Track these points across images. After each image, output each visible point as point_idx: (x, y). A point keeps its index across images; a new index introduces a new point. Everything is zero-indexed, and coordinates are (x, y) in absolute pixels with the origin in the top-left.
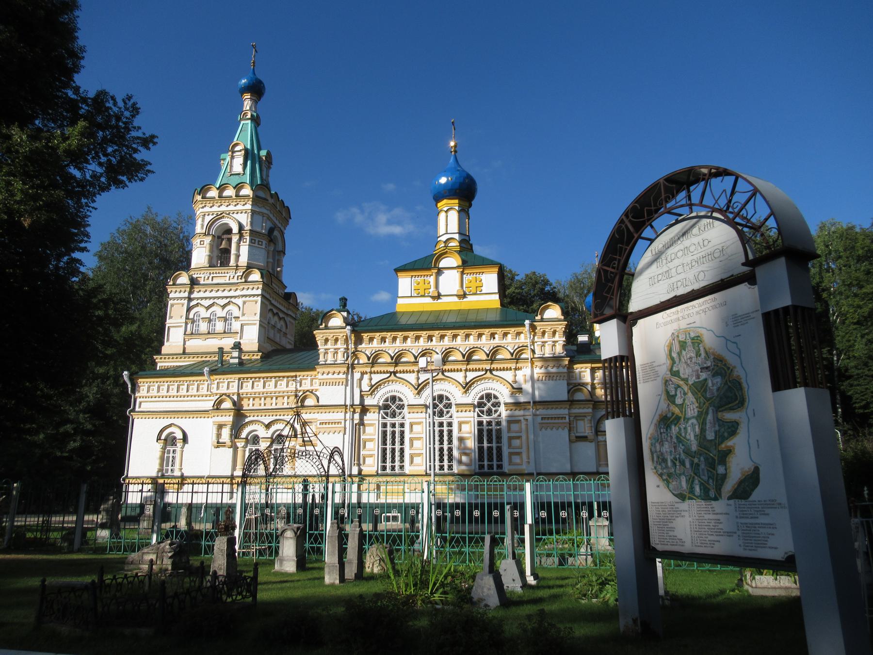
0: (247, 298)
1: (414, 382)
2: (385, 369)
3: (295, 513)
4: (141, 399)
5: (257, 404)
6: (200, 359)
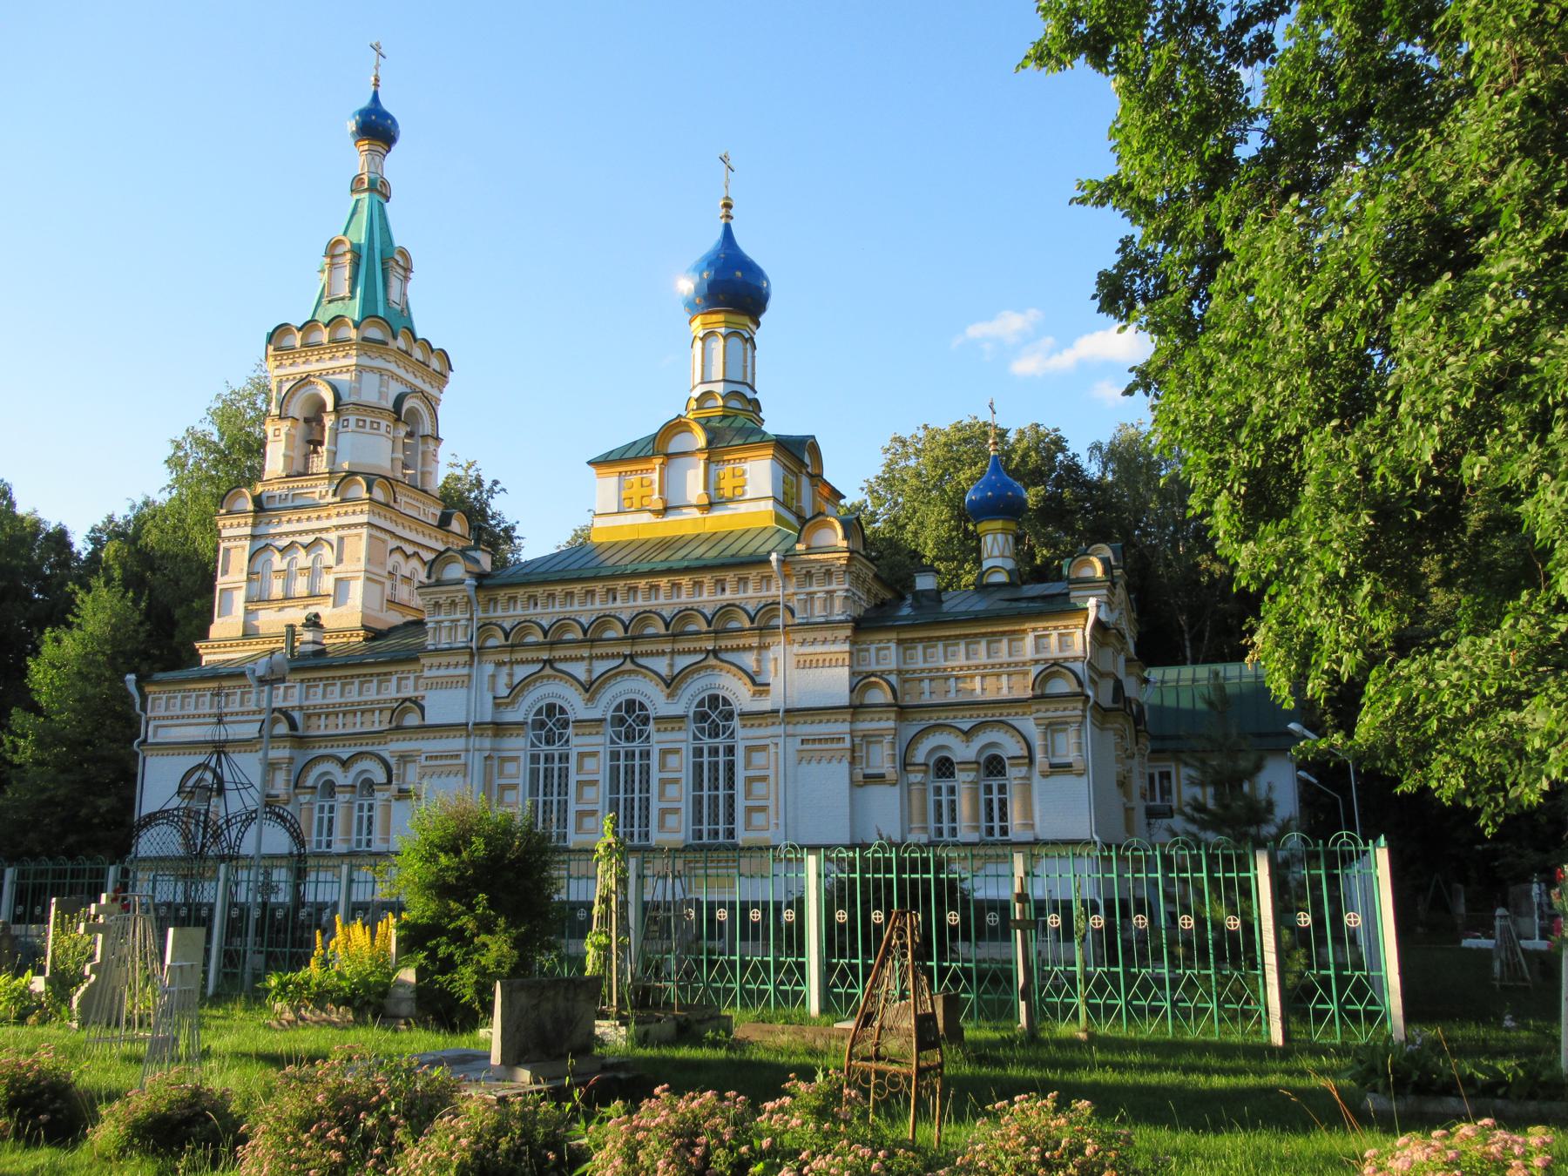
1: (583, 677)
2: (615, 650)
3: (711, 919)
4: (158, 723)
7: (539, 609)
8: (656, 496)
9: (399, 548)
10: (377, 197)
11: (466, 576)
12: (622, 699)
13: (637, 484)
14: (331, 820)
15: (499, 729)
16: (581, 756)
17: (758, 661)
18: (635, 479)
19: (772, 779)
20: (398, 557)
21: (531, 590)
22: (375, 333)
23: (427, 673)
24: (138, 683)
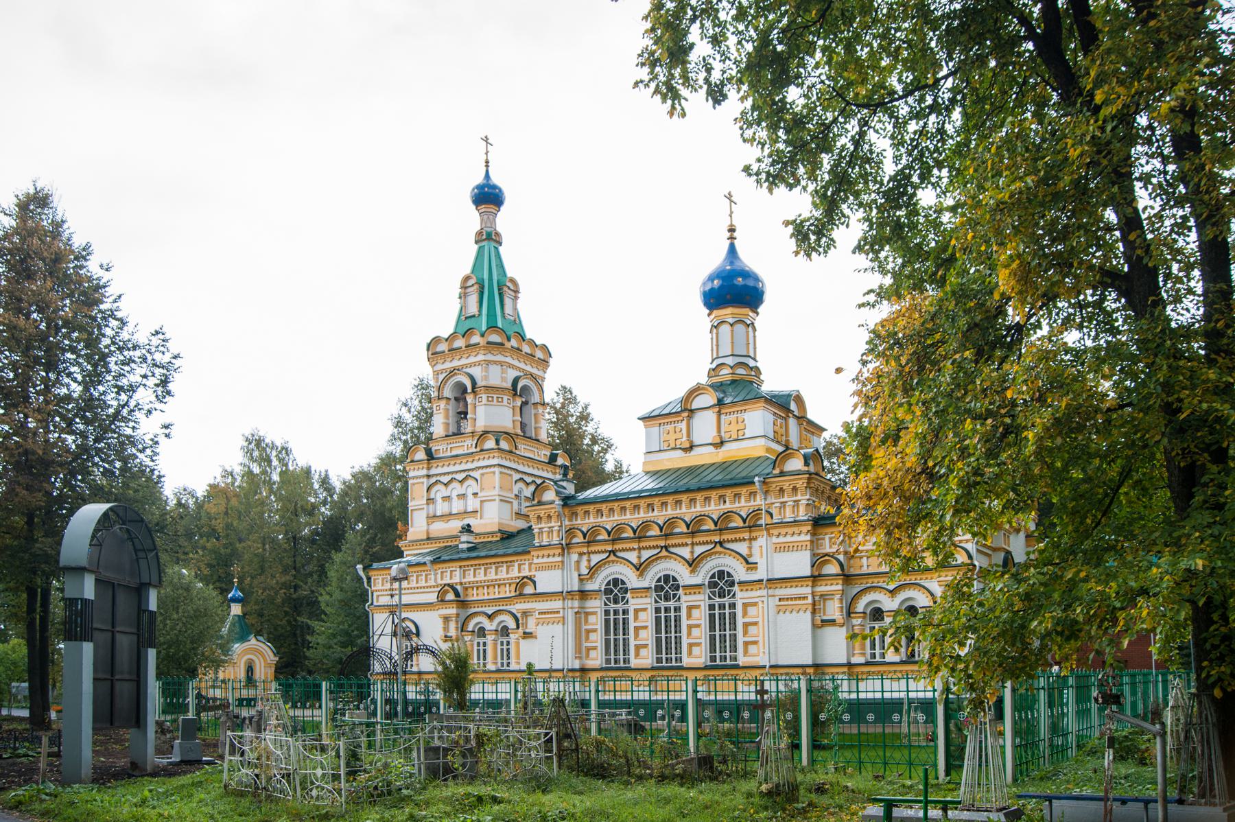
0: (484, 471)
1: (635, 561)
2: (655, 543)
5: (483, 594)
6: (442, 545)
7: (604, 518)
8: (685, 438)
9: (521, 479)
10: (493, 244)
11: (557, 499)
12: (662, 574)
13: (734, 422)
14: (485, 651)
15: (583, 594)
16: (636, 611)
17: (750, 548)
18: (670, 427)
19: (760, 624)
20: (521, 485)
21: (598, 506)
22: (495, 338)
23: (536, 561)
24: (364, 569)
